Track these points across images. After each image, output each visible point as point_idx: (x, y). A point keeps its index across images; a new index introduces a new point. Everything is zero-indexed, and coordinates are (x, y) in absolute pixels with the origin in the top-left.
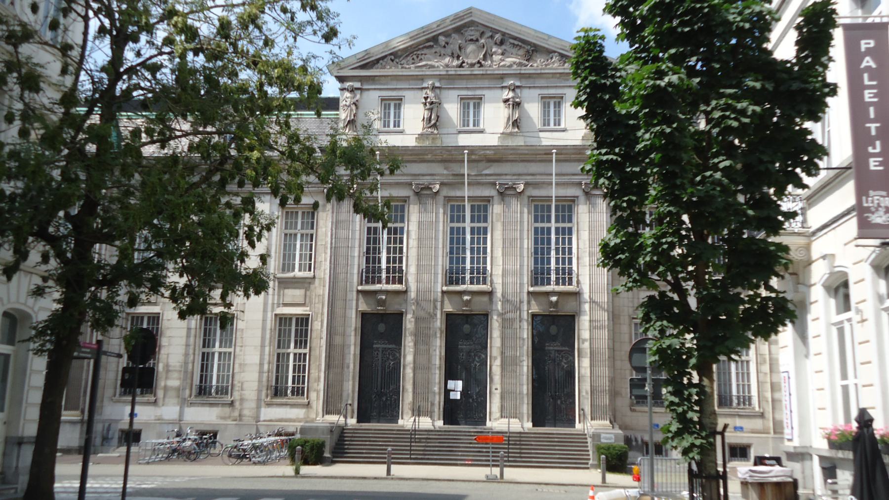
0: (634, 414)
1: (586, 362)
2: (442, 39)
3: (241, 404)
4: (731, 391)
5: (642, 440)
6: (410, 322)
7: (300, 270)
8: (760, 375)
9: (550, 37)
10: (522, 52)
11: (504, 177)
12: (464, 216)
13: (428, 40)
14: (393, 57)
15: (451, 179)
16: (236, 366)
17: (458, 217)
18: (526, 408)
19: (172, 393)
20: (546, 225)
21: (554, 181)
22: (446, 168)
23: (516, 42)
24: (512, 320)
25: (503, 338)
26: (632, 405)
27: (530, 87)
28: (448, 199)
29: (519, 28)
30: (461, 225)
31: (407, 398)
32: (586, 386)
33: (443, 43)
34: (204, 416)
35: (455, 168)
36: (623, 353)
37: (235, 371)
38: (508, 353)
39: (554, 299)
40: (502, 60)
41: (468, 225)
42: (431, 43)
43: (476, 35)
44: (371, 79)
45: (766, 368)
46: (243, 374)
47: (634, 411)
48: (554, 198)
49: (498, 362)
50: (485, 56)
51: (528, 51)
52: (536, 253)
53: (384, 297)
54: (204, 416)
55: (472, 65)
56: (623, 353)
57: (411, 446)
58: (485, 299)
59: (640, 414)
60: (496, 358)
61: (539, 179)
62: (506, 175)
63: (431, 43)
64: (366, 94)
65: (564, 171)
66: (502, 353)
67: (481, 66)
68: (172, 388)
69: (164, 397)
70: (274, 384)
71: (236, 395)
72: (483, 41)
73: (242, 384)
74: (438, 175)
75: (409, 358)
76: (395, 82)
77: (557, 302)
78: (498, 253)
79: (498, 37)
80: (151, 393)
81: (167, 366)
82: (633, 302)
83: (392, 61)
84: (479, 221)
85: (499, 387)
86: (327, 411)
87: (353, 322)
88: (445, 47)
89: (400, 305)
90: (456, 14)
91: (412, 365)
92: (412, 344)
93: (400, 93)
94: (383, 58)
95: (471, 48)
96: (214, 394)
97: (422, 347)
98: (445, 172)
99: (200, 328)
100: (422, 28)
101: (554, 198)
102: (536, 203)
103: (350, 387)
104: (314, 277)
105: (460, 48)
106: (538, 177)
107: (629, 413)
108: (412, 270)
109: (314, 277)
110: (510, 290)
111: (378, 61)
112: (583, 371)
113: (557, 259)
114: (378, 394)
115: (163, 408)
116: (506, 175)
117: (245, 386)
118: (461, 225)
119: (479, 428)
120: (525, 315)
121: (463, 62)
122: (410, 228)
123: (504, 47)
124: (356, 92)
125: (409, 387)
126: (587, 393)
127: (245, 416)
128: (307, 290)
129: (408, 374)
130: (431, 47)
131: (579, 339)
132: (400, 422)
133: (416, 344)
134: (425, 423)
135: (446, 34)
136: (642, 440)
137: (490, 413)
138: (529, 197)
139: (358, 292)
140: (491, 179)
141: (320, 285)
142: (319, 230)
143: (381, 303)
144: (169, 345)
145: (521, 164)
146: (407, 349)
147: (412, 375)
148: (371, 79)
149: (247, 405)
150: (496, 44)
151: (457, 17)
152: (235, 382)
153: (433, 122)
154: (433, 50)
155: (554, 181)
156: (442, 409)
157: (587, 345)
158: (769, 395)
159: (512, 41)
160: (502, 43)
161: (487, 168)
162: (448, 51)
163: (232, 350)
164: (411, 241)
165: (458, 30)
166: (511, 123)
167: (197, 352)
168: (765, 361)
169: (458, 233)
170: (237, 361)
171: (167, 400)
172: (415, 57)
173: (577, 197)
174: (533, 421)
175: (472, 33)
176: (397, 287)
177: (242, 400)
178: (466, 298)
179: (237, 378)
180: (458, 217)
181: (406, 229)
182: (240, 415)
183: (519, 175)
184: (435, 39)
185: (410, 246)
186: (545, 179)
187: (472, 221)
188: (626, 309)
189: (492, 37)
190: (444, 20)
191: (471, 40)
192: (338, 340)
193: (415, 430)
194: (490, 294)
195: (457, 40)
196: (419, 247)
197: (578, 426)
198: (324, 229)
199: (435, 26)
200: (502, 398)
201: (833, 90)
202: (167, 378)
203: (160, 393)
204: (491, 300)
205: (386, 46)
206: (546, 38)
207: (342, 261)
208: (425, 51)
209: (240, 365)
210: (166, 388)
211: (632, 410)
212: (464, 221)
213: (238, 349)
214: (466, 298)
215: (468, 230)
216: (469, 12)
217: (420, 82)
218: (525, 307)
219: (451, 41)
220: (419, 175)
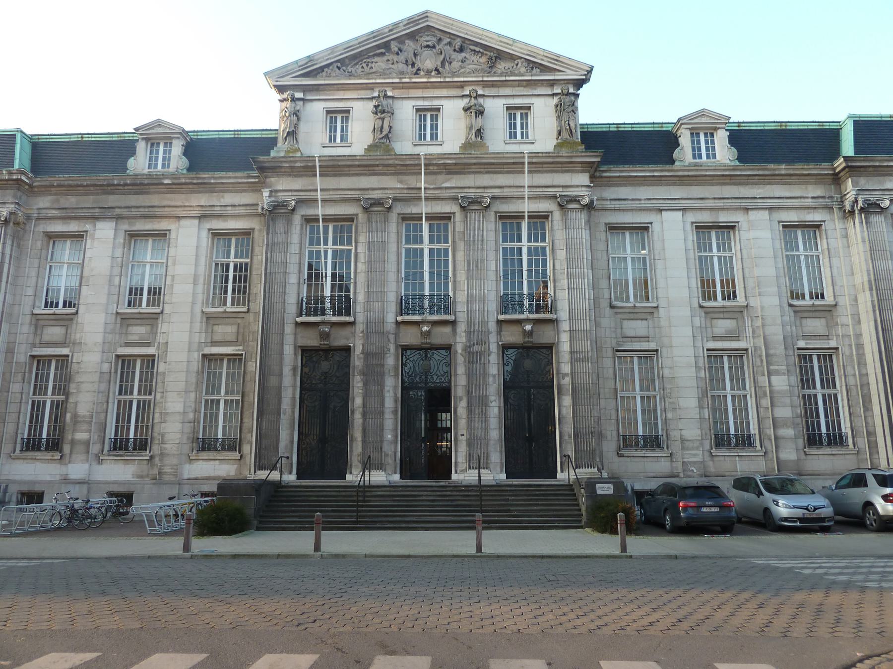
0: (622, 459)
1: (567, 401)
2: (394, 47)
3: (161, 460)
4: (728, 429)
5: (632, 489)
6: (359, 358)
7: (233, 304)
8: (761, 410)
9: (514, 41)
10: (483, 60)
11: (466, 190)
12: (421, 237)
13: (378, 47)
14: (339, 65)
15: (405, 194)
16: (157, 415)
17: (415, 237)
18: (496, 457)
19: (80, 448)
20: (516, 245)
21: (526, 194)
22: (401, 182)
23: (477, 49)
24: (479, 354)
25: (469, 375)
26: (619, 449)
27: (493, 96)
28: (405, 218)
29: (481, 32)
30: (418, 246)
31: (356, 448)
32: (569, 429)
33: (396, 49)
34: (119, 472)
35: (411, 181)
36: (607, 390)
37: (155, 421)
38: (476, 393)
39: (529, 327)
40: (461, 67)
41: (426, 246)
42: (383, 50)
43: (432, 40)
44: (316, 88)
45: (766, 402)
46: (163, 425)
47: (622, 456)
48: (526, 215)
49: (463, 404)
50: (443, 63)
51: (490, 58)
52: (505, 275)
53: (327, 330)
54: (119, 472)
55: (428, 73)
56: (607, 390)
57: (481, 501)
58: (447, 330)
59: (628, 460)
60: (461, 399)
61: (507, 192)
62: (469, 188)
63: (383, 50)
64: (309, 106)
65: (536, 183)
66: (469, 393)
67: (439, 73)
68: (80, 442)
69: (71, 454)
70: (113, 436)
71: (156, 449)
72: (441, 46)
73: (163, 436)
74: (391, 189)
75: (358, 402)
76: (342, 92)
77: (531, 332)
78: (462, 276)
79: (458, 43)
80: (57, 449)
81: (75, 416)
82: (615, 332)
83: (339, 68)
84: (439, 242)
85: (465, 432)
86: (260, 466)
87: (290, 357)
88: (398, 54)
89: (348, 339)
90: (410, 19)
91: (361, 410)
92: (360, 385)
93: (436, 103)
94: (328, 66)
95: (427, 53)
96: (130, 448)
97: (373, 388)
98: (399, 186)
99: (116, 372)
100: (373, 32)
101: (526, 215)
102: (408, 222)
103: (287, 438)
104: (162, 312)
105: (415, 55)
106: (506, 190)
107: (617, 459)
108: (361, 297)
109: (162, 312)
110: (477, 318)
111: (322, 69)
112: (564, 411)
113: (333, 286)
114: (324, 446)
115: (70, 465)
116: (469, 188)
117: (167, 437)
118: (418, 246)
119: (443, 483)
120: (493, 347)
121: (419, 69)
122: (359, 250)
123: (463, 54)
124: (298, 103)
125: (358, 434)
126: (570, 437)
127: (166, 474)
128: (67, 327)
129: (357, 419)
130: (383, 54)
131: (558, 374)
132: (349, 477)
133: (366, 384)
134: (378, 477)
135: (400, 40)
136: (632, 489)
137: (456, 463)
138: (496, 213)
139: (297, 324)
140: (452, 193)
141: (255, 319)
142: (255, 257)
143: (325, 336)
144: (79, 392)
145: (486, 176)
146: (356, 390)
147: (361, 421)
148: (316, 88)
149: (168, 461)
150: (455, 50)
151: (412, 21)
152: (155, 435)
153: (384, 133)
154: (385, 58)
155: (526, 194)
156: (398, 461)
157: (567, 381)
158: (771, 432)
159: (472, 47)
160: (461, 50)
161: (446, 181)
162: (402, 57)
163: (152, 397)
164: (360, 265)
165: (412, 36)
166: (473, 131)
167: (111, 400)
168: (765, 394)
169: (415, 256)
170: (157, 410)
171: (74, 456)
172: (364, 65)
173: (551, 212)
174: (401, 474)
175: (426, 39)
176: (347, 319)
177: (162, 455)
178: (425, 328)
179: (156, 429)
180: (415, 237)
181: (353, 251)
182: (160, 473)
183: (485, 187)
184: (386, 45)
185: (358, 270)
186: (414, 194)
187: (431, 241)
188: (608, 340)
189: (450, 44)
190: (396, 25)
191: (428, 46)
192: (273, 381)
193: (364, 486)
194: (453, 323)
195: (410, 45)
196: (370, 271)
197: (560, 475)
198: (260, 257)
199: (387, 30)
200: (470, 445)
201: (553, 89)
202: (74, 431)
203: (66, 448)
204: (454, 331)
205: (332, 53)
206: (511, 42)
207: (277, 288)
208: (376, 59)
209: (161, 413)
210: (73, 443)
211: (620, 456)
212: (421, 242)
213: (158, 395)
214: (425, 328)
215: (525, 251)
216: (425, 16)
217: (369, 92)
218: (493, 338)
219: (405, 48)
220: (368, 189)
